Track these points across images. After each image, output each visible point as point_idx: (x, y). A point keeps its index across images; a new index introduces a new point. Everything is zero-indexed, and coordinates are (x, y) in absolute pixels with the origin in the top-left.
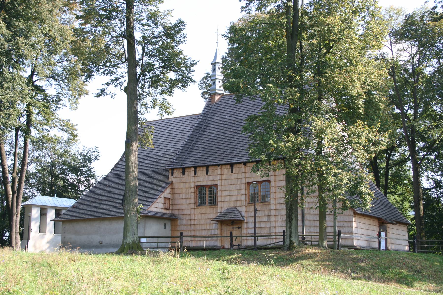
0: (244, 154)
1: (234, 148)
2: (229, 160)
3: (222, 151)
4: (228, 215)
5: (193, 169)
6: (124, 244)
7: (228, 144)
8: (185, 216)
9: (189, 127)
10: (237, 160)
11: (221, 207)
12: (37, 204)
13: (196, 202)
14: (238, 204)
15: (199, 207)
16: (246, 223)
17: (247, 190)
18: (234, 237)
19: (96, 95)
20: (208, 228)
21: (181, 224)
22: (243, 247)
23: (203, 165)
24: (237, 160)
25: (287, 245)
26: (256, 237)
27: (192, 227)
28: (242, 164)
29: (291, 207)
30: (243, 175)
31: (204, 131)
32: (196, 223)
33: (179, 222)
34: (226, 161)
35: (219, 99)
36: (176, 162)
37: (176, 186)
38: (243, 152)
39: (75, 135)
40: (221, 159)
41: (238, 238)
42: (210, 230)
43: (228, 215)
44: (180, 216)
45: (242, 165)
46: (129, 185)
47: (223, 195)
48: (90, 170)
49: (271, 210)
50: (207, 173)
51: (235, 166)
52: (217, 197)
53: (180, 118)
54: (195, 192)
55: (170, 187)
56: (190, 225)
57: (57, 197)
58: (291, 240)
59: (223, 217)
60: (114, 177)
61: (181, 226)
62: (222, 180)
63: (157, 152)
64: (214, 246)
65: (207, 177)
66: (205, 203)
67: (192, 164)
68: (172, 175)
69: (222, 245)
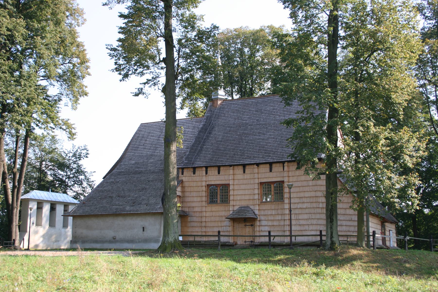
0: (256, 155)
1: (244, 150)
2: (242, 161)
3: (232, 152)
4: (242, 213)
5: (204, 169)
6: (166, 242)
7: (238, 146)
8: (195, 213)
9: (191, 129)
10: (250, 161)
11: (234, 206)
12: (74, 202)
13: (207, 200)
14: (251, 202)
15: (210, 205)
16: (259, 221)
17: (259, 190)
18: (272, 236)
19: (134, 94)
20: (220, 225)
21: (192, 221)
22: (257, 244)
23: (215, 165)
24: (250, 161)
25: (328, 245)
26: (291, 236)
27: (204, 224)
28: (255, 165)
29: (332, 208)
30: (256, 176)
31: (210, 133)
32: (207, 220)
33: (189, 219)
34: (238, 162)
35: (220, 104)
36: (186, 161)
37: (186, 184)
38: (254, 154)
39: (73, 134)
40: (233, 160)
41: (276, 237)
42: (221, 226)
43: (242, 213)
44: (191, 213)
45: (255, 166)
46: (169, 184)
47: (235, 194)
48: (79, 166)
49: (284, 209)
50: (219, 173)
51: (247, 167)
52: (229, 196)
53: (180, 121)
54: (206, 190)
55: (181, 185)
56: (201, 222)
57: (51, 192)
58: (333, 240)
59: (237, 215)
60: (119, 175)
61: (191, 223)
62: (234, 180)
63: (161, 151)
64: (227, 242)
65: (218, 176)
66: (217, 201)
67: (204, 164)
68: (183, 174)
69: (234, 242)
